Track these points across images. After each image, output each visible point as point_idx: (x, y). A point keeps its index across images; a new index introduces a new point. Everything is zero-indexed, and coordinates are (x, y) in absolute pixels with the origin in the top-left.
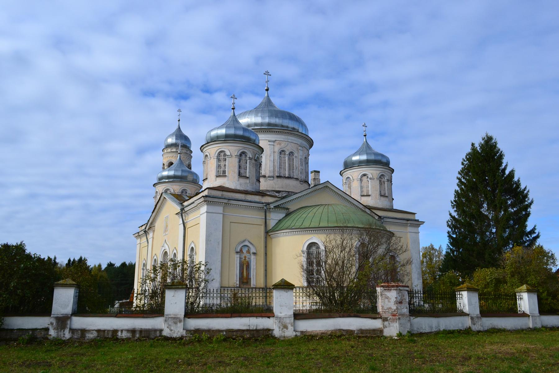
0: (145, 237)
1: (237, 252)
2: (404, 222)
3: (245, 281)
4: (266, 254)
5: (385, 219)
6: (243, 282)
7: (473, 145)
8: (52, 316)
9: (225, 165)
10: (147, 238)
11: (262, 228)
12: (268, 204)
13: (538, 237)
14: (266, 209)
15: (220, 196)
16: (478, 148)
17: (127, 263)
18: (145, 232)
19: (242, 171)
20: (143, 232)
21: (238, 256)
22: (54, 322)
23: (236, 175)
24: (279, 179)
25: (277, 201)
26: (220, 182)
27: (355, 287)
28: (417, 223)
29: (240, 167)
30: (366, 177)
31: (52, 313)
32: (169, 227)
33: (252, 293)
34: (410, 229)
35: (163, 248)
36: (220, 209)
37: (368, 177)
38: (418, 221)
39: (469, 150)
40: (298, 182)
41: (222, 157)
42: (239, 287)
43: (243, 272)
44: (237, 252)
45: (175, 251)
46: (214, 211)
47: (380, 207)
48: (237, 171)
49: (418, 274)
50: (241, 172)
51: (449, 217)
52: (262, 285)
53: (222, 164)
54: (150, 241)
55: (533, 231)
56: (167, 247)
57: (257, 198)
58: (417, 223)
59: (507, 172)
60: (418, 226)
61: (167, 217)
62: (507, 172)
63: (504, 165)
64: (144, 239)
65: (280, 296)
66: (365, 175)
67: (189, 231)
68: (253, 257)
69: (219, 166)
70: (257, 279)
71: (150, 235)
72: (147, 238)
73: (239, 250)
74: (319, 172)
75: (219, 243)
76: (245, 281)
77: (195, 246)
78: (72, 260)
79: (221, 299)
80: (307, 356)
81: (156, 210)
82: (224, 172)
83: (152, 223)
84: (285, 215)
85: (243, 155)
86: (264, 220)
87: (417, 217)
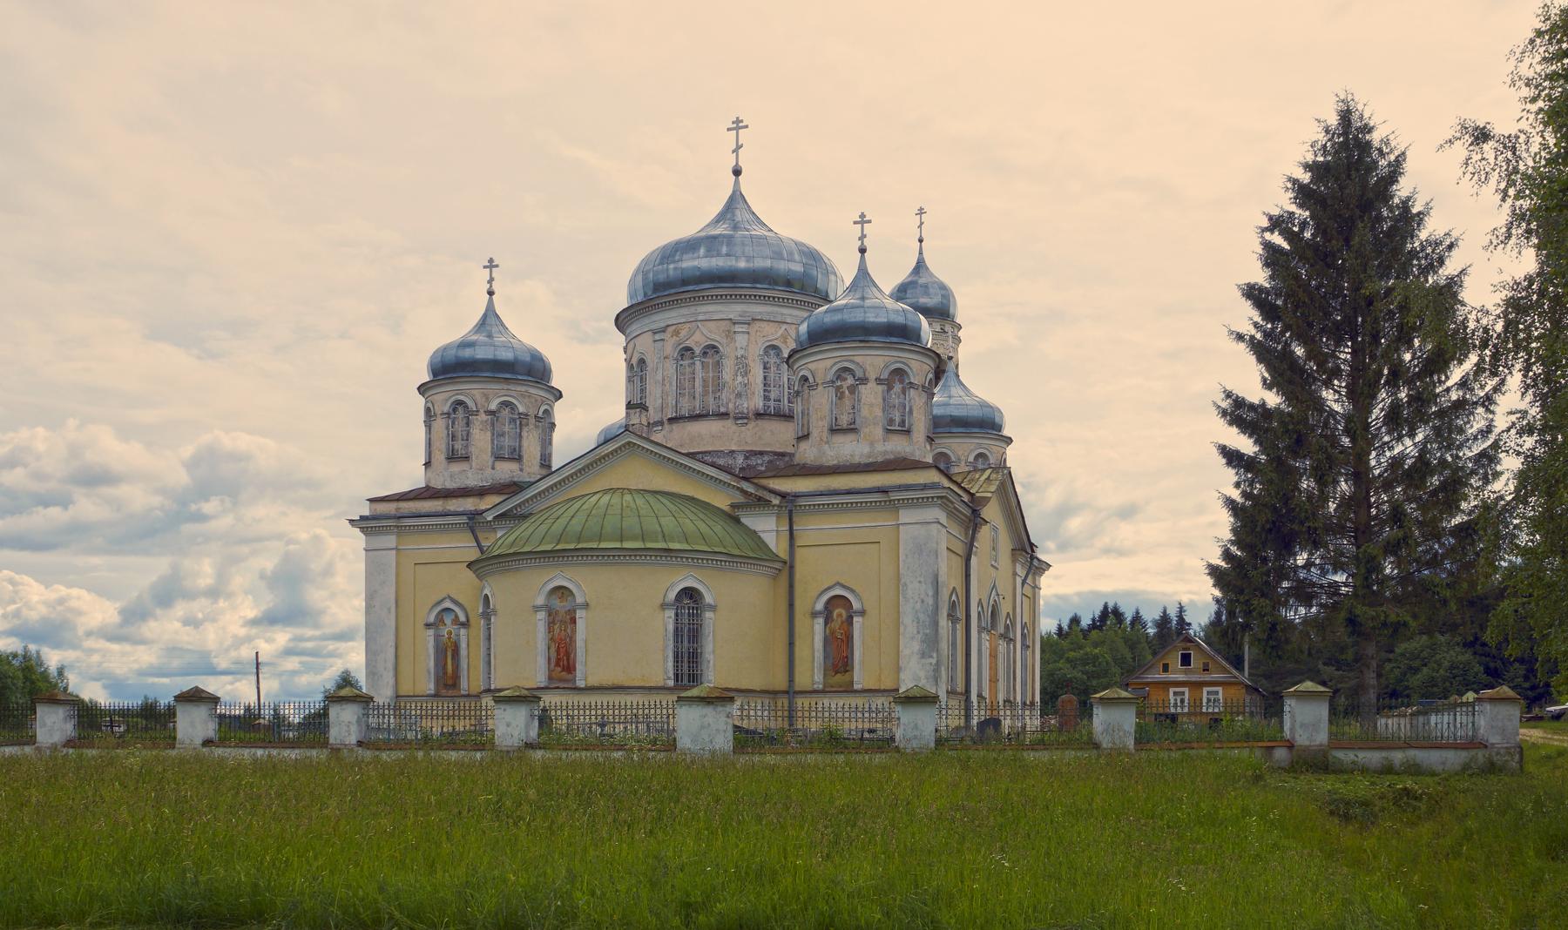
1: (428, 625)
5: (802, 502)
6: (446, 686)
19: (458, 445)
21: (431, 632)
24: (675, 426)
36: (390, 540)
44: (428, 625)
47: (865, 461)
52: (780, 682)
68: (463, 631)
70: (471, 680)
73: (432, 619)
80: (1314, 892)
85: (460, 409)
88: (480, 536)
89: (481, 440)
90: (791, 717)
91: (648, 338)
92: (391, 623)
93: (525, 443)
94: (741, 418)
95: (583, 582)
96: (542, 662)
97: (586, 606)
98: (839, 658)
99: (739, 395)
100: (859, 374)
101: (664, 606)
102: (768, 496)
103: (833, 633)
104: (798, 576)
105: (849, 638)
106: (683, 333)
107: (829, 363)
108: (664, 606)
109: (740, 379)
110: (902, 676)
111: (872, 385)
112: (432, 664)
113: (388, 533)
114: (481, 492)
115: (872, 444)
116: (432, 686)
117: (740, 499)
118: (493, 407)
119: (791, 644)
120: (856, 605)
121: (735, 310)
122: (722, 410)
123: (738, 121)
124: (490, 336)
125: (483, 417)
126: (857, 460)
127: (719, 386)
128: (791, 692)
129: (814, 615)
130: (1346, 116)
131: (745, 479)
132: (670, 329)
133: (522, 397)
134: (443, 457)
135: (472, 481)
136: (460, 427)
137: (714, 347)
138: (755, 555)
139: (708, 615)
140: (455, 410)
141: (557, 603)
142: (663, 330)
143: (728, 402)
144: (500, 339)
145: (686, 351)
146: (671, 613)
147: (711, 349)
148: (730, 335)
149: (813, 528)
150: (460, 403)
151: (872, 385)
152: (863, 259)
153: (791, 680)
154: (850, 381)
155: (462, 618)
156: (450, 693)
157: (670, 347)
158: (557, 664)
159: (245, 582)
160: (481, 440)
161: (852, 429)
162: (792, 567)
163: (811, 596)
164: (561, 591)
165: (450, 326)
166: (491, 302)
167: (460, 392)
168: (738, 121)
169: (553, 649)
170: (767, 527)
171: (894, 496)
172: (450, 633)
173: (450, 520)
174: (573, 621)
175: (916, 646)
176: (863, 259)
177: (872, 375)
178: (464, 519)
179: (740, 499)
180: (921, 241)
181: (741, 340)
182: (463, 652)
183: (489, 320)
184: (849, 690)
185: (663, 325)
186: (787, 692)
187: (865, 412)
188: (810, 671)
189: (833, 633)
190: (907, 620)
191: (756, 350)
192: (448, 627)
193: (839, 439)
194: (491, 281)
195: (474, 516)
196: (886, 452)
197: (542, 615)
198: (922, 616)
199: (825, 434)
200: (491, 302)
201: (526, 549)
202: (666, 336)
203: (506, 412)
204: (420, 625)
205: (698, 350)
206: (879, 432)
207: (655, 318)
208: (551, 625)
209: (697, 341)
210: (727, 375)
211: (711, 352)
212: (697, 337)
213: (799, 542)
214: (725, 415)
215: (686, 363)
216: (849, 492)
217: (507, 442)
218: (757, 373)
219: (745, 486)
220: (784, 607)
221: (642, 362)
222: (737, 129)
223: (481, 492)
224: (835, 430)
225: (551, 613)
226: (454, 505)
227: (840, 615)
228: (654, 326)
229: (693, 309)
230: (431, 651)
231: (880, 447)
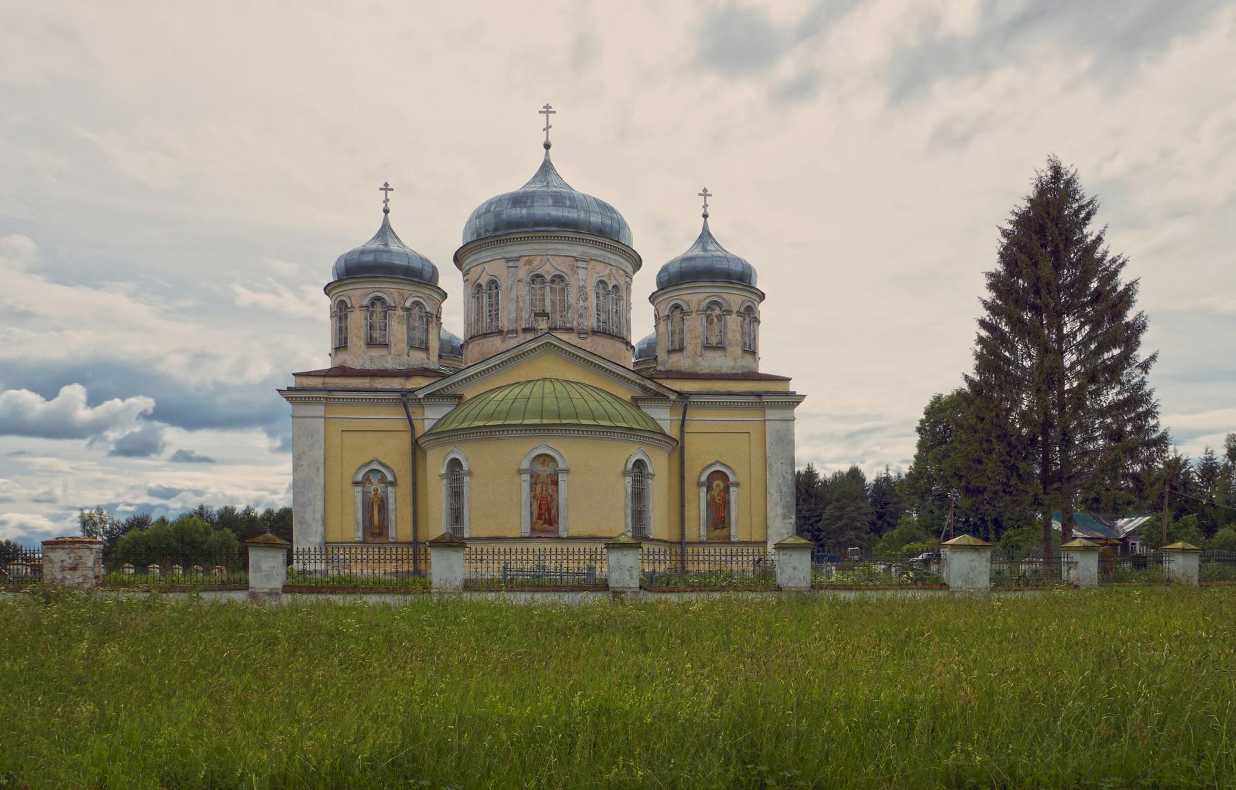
1: (356, 483)
3: (377, 531)
4: (415, 484)
5: (693, 399)
6: (373, 534)
7: (966, 377)
14: (406, 399)
16: (977, 378)
19: (377, 334)
21: (359, 489)
27: (1135, 477)
28: (794, 400)
29: (371, 327)
33: (344, 554)
34: (771, 414)
38: (793, 394)
42: (364, 542)
43: (372, 516)
44: (356, 483)
47: (729, 371)
49: (784, 507)
52: (410, 539)
58: (794, 400)
68: (390, 489)
73: (359, 477)
75: (318, 470)
85: (378, 305)
87: (793, 387)
88: (411, 410)
89: (398, 331)
90: (682, 561)
91: (501, 264)
92: (321, 480)
93: (430, 337)
94: (582, 333)
95: (566, 451)
96: (526, 514)
97: (567, 471)
98: (719, 516)
99: (581, 316)
100: (725, 307)
101: (625, 473)
102: (666, 393)
103: (713, 499)
104: (686, 456)
105: (726, 504)
106: (535, 263)
107: (702, 296)
108: (625, 473)
109: (582, 303)
110: (769, 532)
111: (734, 316)
112: (360, 516)
114: (407, 374)
115: (735, 360)
116: (360, 534)
117: (639, 393)
118: (408, 304)
119: (682, 506)
120: (732, 479)
121: (578, 250)
122: (569, 326)
123: (547, 107)
124: (386, 245)
125: (400, 312)
126: (724, 370)
127: (565, 308)
128: (682, 543)
129: (699, 484)
130: (1057, 172)
131: (650, 379)
132: (524, 259)
133: (734, 298)
134: (362, 343)
135: (390, 363)
136: (377, 318)
137: (560, 276)
138: (656, 435)
139: (466, 479)
140: (373, 304)
141: (539, 468)
142: (517, 259)
143: (572, 319)
144: (393, 247)
145: (537, 278)
146: (629, 479)
147: (559, 278)
148: (574, 269)
149: (699, 419)
150: (378, 299)
151: (734, 316)
152: (705, 222)
153: (683, 534)
154: (717, 311)
155: (390, 478)
156: (377, 540)
157: (523, 272)
158: (539, 518)
160: (398, 331)
161: (720, 347)
162: (682, 448)
163: (696, 469)
164: (544, 458)
165: (358, 235)
166: (705, 224)
168: (547, 107)
169: (535, 506)
170: (664, 417)
171: (765, 399)
174: (556, 483)
175: (779, 510)
176: (705, 222)
178: (397, 395)
179: (639, 393)
181: (581, 273)
182: (391, 507)
183: (385, 231)
184: (727, 541)
186: (680, 543)
187: (730, 336)
188: (697, 527)
189: (713, 499)
190: (772, 490)
191: (593, 282)
192: (375, 485)
193: (710, 354)
194: (386, 201)
195: (405, 393)
196: (743, 367)
197: (526, 477)
198: (784, 489)
199: (699, 350)
200: (705, 224)
201: (465, 425)
202: (520, 263)
203: (416, 311)
205: (548, 278)
206: (739, 351)
207: (507, 249)
208: (533, 485)
209: (548, 271)
210: (572, 298)
211: (558, 280)
212: (547, 267)
213: (687, 429)
215: (537, 286)
216: (730, 394)
217: (418, 334)
218: (593, 300)
219: (648, 383)
220: (676, 478)
221: (493, 284)
222: (548, 113)
223: (407, 374)
224: (708, 347)
225: (535, 480)
226: (380, 383)
227: (718, 486)
228: (508, 255)
229: (543, 246)
230: (360, 505)
231: (740, 363)
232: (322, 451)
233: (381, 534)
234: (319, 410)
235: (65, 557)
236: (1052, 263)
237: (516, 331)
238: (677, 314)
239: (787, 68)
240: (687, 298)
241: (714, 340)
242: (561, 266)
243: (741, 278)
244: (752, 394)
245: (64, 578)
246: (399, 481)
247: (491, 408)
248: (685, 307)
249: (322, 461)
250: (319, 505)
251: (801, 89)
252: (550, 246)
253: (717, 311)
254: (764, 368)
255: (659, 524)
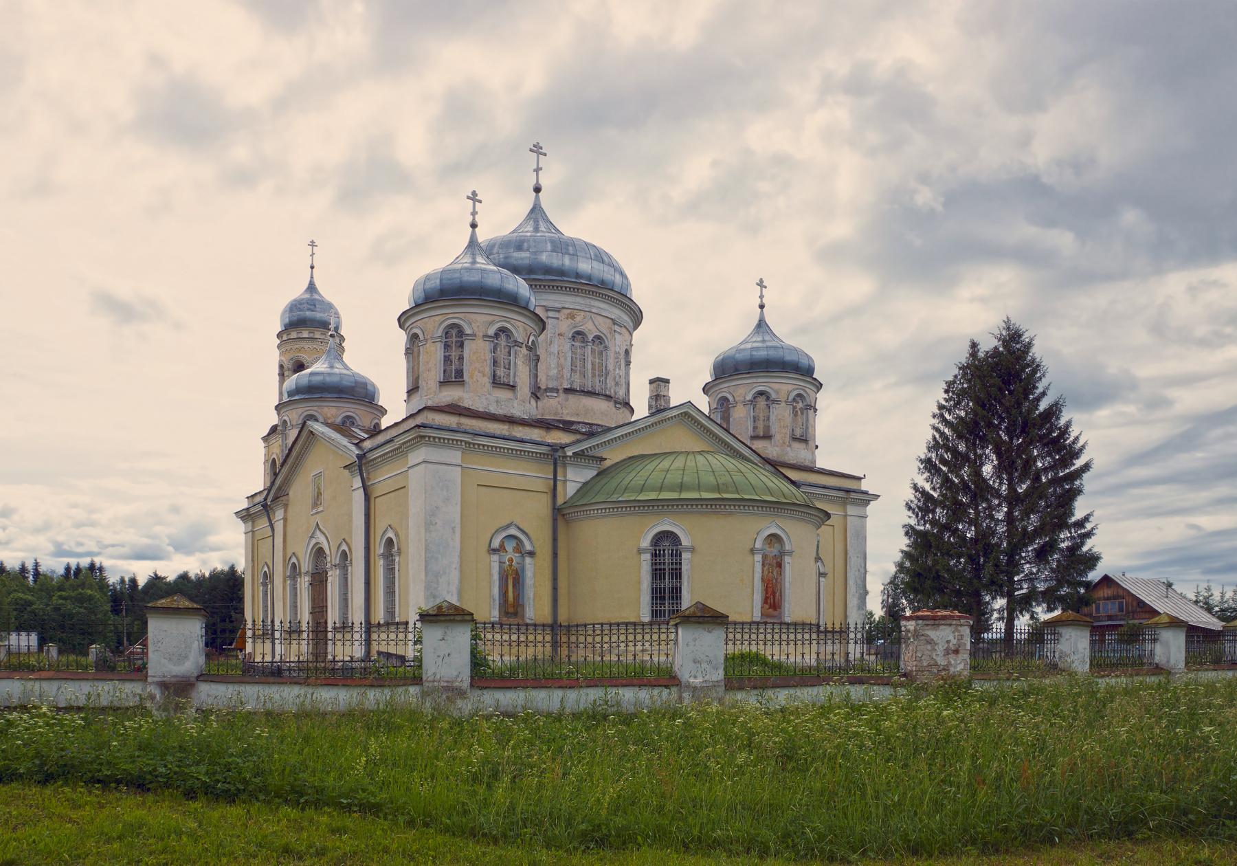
0: (266, 519)
2: (841, 494)
3: (511, 610)
8: (149, 679)
9: (461, 358)
10: (270, 521)
11: (546, 500)
12: (563, 447)
13: (1089, 535)
14: (555, 457)
15: (454, 426)
17: (192, 575)
18: (265, 506)
19: (501, 372)
20: (260, 507)
21: (495, 558)
22: (157, 692)
23: (487, 381)
24: (570, 396)
25: (578, 441)
26: (449, 395)
28: (866, 498)
29: (495, 363)
30: (764, 397)
31: (150, 672)
32: (326, 495)
34: (851, 510)
35: (314, 541)
37: (768, 398)
38: (866, 493)
39: (963, 357)
40: (611, 404)
41: (454, 339)
42: (651, 624)
45: (344, 547)
46: (442, 460)
48: (488, 370)
50: (498, 373)
51: (910, 495)
52: (549, 620)
53: (454, 354)
54: (279, 526)
55: (1080, 524)
56: (322, 539)
57: (535, 434)
58: (866, 498)
59: (1043, 405)
60: (867, 502)
61: (319, 475)
62: (1043, 405)
63: (1038, 392)
64: (263, 523)
65: (695, 640)
66: (761, 393)
67: (380, 505)
68: (528, 560)
69: (447, 359)
71: (279, 514)
72: (270, 521)
73: (496, 544)
74: (667, 381)
75: (453, 529)
76: (511, 610)
77: (397, 535)
78: (73, 567)
79: (254, 642)
81: (290, 461)
82: (460, 373)
83: (280, 488)
84: (595, 473)
85: (503, 336)
86: (552, 482)
87: (865, 486)
92: (457, 543)
106: (578, 319)
113: (456, 448)
135: (517, 411)
136: (501, 353)
140: (497, 335)
142: (558, 310)
145: (579, 335)
159: (153, 476)
166: (762, 313)
167: (507, 319)
172: (511, 560)
173: (528, 447)
174: (780, 565)
177: (783, 404)
180: (312, 267)
185: (560, 306)
195: (556, 448)
199: (787, 440)
200: (762, 313)
202: (562, 315)
204: (830, 575)
207: (545, 296)
209: (590, 329)
214: (609, 397)
215: (577, 344)
216: (824, 487)
229: (588, 301)
230: (496, 577)
232: (459, 508)
233: (515, 614)
234: (455, 456)
235: (951, 638)
236: (1001, 403)
237: (557, 391)
238: (762, 402)
239: (241, 153)
240: (776, 386)
241: (798, 433)
242: (603, 326)
243: (802, 370)
244: (839, 489)
245: (949, 664)
246: (538, 551)
247: (656, 478)
248: (774, 396)
249: (458, 520)
250: (455, 576)
251: (242, 179)
252: (594, 303)
253: (800, 405)
254: (820, 464)
255: (537, 608)
